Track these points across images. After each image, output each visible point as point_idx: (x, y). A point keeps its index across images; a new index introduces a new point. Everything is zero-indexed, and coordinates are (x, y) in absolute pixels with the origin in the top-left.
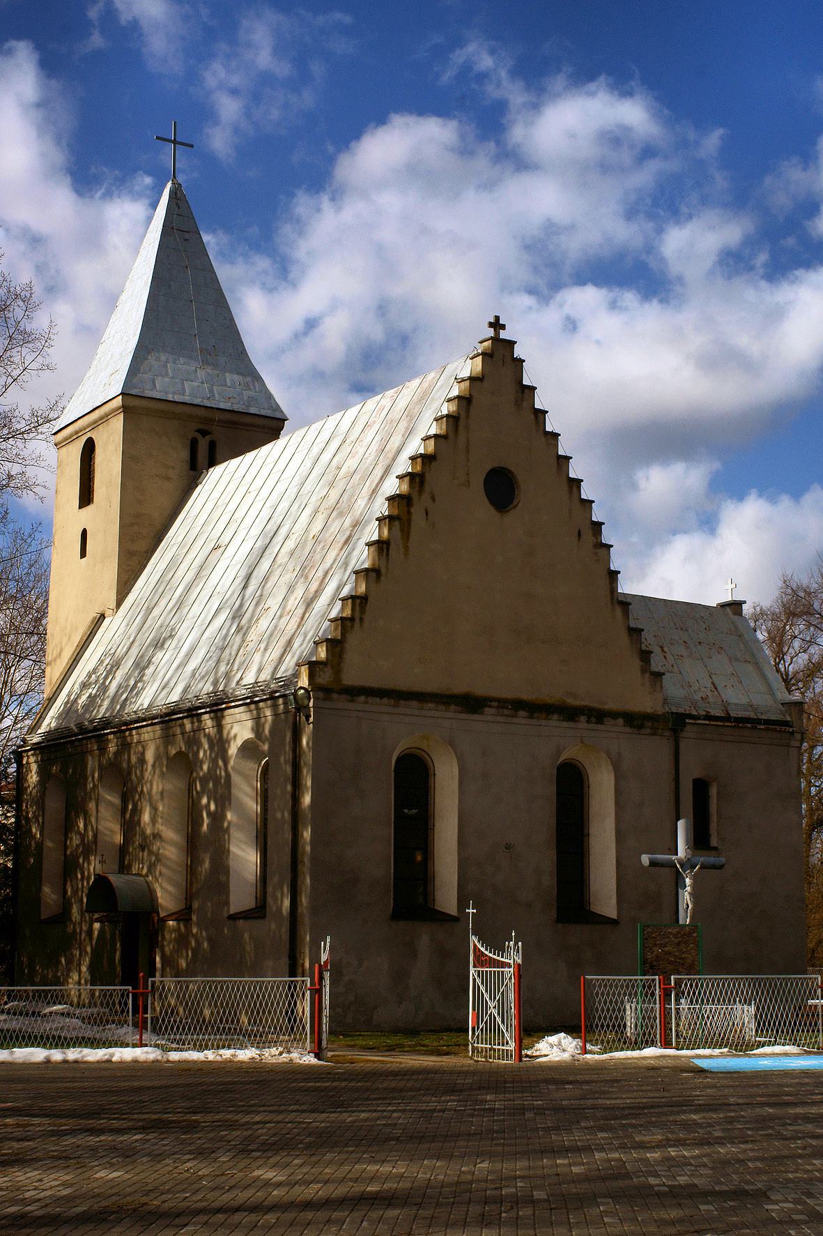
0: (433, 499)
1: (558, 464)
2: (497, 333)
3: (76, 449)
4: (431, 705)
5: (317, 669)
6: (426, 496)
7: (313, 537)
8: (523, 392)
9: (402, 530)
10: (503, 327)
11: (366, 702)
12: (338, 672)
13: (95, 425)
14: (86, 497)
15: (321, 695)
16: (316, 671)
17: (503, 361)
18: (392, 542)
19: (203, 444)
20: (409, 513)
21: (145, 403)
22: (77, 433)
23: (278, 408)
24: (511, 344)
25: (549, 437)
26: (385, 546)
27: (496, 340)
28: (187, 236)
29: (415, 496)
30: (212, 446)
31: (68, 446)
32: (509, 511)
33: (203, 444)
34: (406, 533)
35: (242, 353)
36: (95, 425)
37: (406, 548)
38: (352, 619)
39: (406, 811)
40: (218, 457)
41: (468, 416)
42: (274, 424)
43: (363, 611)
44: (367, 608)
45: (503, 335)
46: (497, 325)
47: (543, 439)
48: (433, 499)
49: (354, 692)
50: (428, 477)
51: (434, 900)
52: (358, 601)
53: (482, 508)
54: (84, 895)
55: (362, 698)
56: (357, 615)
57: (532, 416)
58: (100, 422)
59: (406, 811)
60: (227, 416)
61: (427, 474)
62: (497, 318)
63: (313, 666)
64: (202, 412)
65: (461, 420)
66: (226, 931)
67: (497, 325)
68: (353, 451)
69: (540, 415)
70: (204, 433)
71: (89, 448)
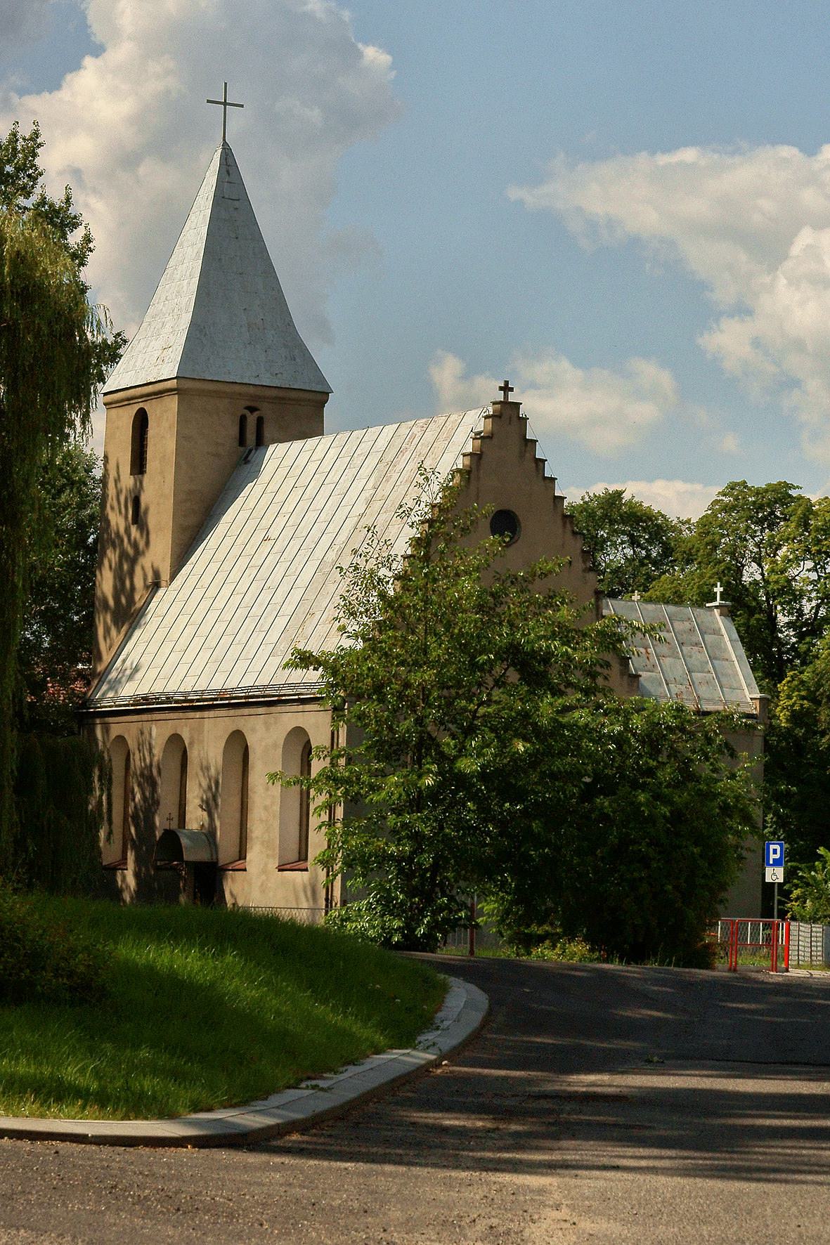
2: (506, 396)
3: (128, 415)
8: (526, 445)
14: (139, 464)
19: (252, 420)
21: (198, 385)
22: (128, 399)
23: (323, 380)
25: (548, 481)
27: (505, 403)
28: (237, 204)
30: (260, 421)
31: (120, 410)
33: (252, 420)
35: (289, 325)
40: (267, 434)
41: (478, 470)
42: (319, 397)
45: (512, 398)
54: (98, 793)
57: (534, 465)
60: (274, 393)
62: (507, 383)
64: (252, 390)
67: (506, 388)
68: (388, 475)
70: (252, 409)
71: (141, 422)
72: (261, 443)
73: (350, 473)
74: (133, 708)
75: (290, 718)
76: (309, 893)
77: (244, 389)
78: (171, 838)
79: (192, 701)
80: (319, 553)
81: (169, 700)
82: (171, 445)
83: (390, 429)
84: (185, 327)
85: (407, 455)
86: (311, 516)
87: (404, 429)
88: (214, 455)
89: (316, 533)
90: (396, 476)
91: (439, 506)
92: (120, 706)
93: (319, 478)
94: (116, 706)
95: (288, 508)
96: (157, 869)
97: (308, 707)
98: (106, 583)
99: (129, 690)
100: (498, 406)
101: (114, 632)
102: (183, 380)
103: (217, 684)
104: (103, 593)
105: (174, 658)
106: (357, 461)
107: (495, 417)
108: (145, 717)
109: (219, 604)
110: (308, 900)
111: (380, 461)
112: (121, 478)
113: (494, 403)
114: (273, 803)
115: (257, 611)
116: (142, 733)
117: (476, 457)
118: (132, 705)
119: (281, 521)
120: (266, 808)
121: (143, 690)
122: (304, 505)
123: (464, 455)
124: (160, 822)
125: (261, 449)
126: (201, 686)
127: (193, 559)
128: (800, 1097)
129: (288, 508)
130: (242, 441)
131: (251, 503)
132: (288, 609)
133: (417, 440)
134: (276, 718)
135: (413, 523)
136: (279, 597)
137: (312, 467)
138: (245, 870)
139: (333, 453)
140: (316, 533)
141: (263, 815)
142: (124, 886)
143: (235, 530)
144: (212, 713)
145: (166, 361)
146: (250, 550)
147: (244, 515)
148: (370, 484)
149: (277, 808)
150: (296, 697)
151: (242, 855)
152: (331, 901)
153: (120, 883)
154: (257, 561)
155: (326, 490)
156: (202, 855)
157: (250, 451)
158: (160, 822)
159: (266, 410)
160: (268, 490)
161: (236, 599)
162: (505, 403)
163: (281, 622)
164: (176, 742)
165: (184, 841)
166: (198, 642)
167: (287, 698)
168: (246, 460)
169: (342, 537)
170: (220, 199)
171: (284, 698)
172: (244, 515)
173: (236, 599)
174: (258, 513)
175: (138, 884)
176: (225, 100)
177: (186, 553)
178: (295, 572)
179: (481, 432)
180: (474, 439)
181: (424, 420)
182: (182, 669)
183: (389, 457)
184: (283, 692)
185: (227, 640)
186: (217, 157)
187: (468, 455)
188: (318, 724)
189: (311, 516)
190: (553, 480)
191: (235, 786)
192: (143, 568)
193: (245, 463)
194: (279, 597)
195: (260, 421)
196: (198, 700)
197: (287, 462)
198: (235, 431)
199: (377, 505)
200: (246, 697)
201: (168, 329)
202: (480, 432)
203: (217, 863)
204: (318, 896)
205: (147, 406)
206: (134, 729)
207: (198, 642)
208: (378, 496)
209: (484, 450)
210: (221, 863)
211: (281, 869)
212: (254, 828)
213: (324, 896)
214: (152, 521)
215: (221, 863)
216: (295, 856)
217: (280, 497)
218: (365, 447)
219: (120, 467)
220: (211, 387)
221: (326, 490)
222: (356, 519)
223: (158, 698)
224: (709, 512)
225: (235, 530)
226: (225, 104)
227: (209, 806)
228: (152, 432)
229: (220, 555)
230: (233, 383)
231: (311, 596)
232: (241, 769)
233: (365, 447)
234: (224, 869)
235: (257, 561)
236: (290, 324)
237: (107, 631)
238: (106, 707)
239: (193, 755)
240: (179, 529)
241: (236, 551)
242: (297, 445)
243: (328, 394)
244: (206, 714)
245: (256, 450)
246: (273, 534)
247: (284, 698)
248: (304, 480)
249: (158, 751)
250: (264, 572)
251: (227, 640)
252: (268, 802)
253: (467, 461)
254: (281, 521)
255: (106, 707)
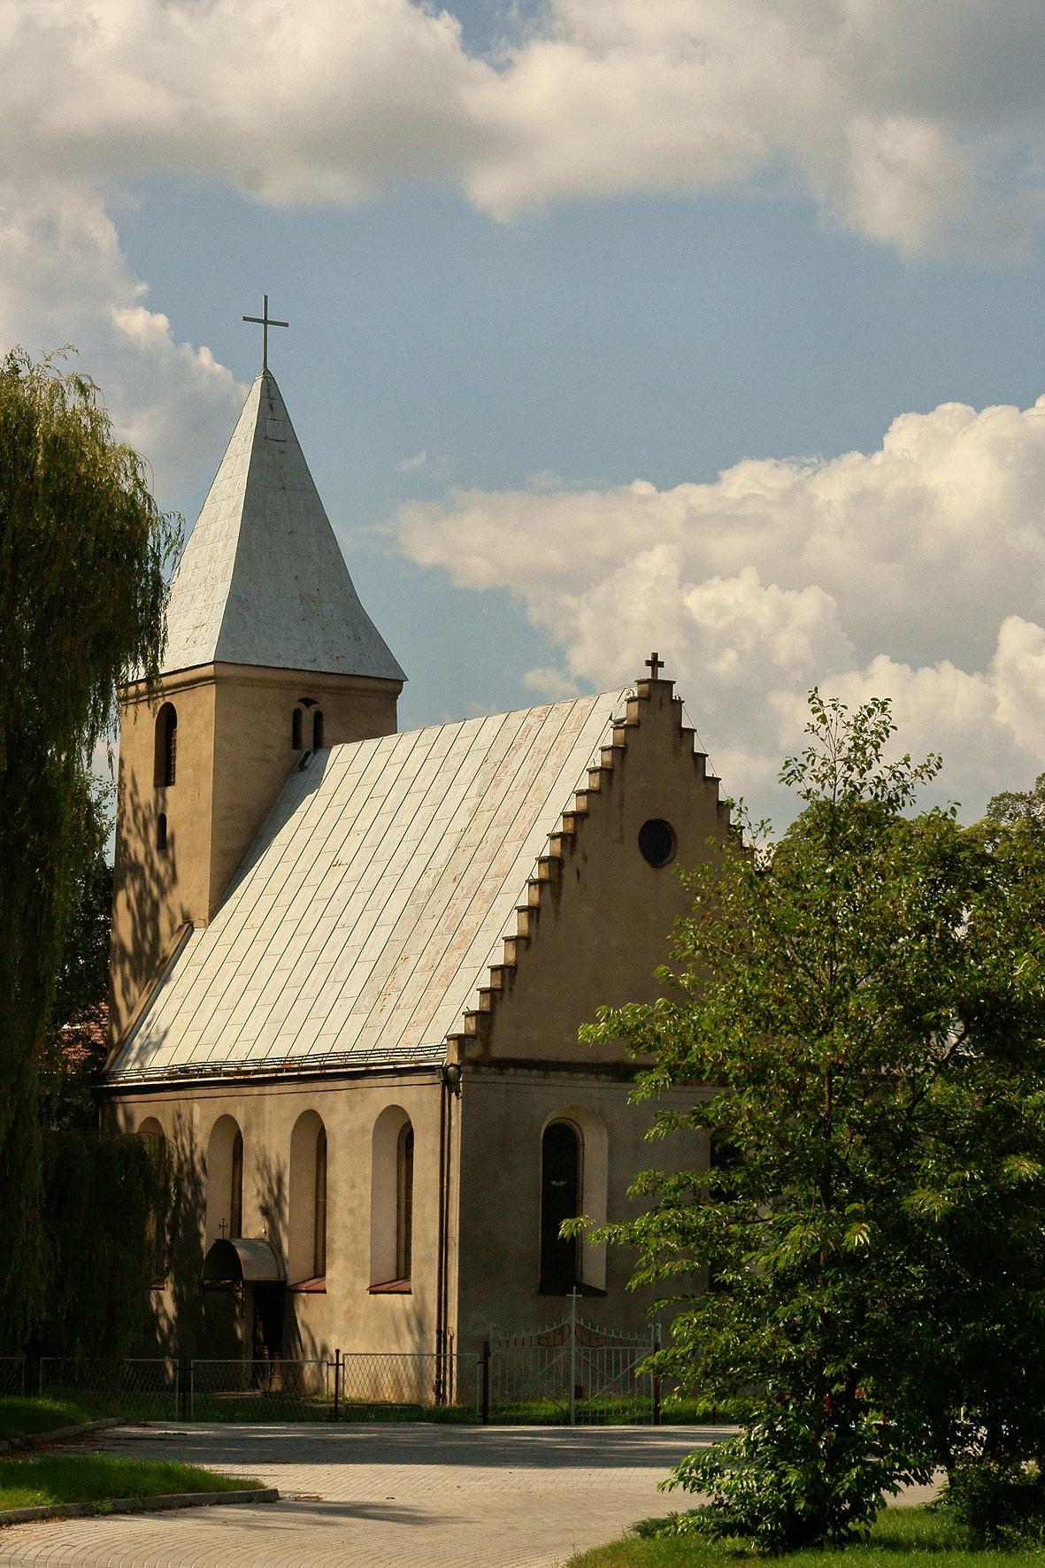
0: (585, 859)
1: (718, 812)
2: (654, 673)
4: (581, 1075)
5: (467, 1043)
6: (578, 857)
7: (455, 879)
8: (681, 736)
9: (552, 893)
10: (661, 665)
11: (515, 1075)
12: (487, 1045)
13: (176, 690)
14: (165, 773)
15: (470, 1068)
16: (465, 1044)
17: (661, 704)
18: (542, 908)
19: (308, 715)
20: (560, 876)
24: (670, 684)
26: (535, 913)
27: (654, 682)
29: (567, 856)
30: (318, 717)
32: (665, 865)
33: (308, 715)
34: (557, 898)
36: (176, 690)
37: (557, 912)
38: (502, 990)
39: (554, 1183)
40: (327, 734)
42: (390, 686)
43: (512, 981)
44: (518, 977)
45: (663, 674)
46: (655, 663)
47: (703, 785)
48: (585, 859)
49: (502, 1065)
50: (580, 837)
51: (582, 1273)
52: (507, 971)
53: (639, 866)
55: (512, 1071)
56: (507, 988)
57: (692, 761)
58: (183, 688)
59: (554, 1183)
61: (579, 834)
62: (655, 656)
63: (460, 1040)
64: (307, 678)
65: (616, 772)
66: (203, 1312)
69: (699, 759)
70: (308, 702)
72: (320, 744)
73: (444, 779)
74: (168, 1082)
75: (382, 1095)
76: (414, 1323)
77: (296, 677)
78: (224, 1251)
79: (248, 1072)
80: (409, 880)
81: (216, 1072)
82: (207, 747)
83: (495, 721)
84: (222, 599)
85: (522, 752)
86: (395, 834)
87: (515, 719)
88: (262, 760)
89: (403, 854)
90: (508, 779)
91: (574, 815)
92: (151, 1080)
93: (402, 786)
94: (146, 1080)
95: (363, 824)
96: (205, 1288)
97: (406, 1080)
98: (124, 928)
99: (160, 1060)
100: (645, 686)
101: (134, 989)
102: (221, 666)
103: (280, 1051)
104: (119, 937)
105: (220, 1017)
106: (454, 762)
107: (642, 700)
108: (182, 1094)
109: (277, 947)
110: (411, 1332)
111: (485, 761)
112: (139, 787)
113: (639, 682)
114: (361, 1206)
115: (329, 955)
116: (179, 1116)
117: (619, 751)
118: (167, 1079)
119: (354, 842)
120: (351, 1211)
121: (181, 1059)
122: (384, 820)
123: (603, 749)
124: (208, 1233)
125: (321, 753)
126: (258, 1053)
127: (239, 891)
128: (533, 1431)
129: (363, 824)
130: (296, 742)
131: (312, 820)
132: (372, 952)
133: (533, 734)
134: (362, 1095)
135: (808, 791)
136: (358, 938)
137: (392, 773)
138: (324, 1292)
139: (419, 754)
140: (403, 854)
141: (348, 1220)
142: (161, 1311)
143: (292, 855)
144: (275, 1089)
145: (199, 642)
146: (315, 878)
147: (303, 835)
148: (474, 789)
149: (366, 1211)
150: (392, 1067)
151: (319, 1271)
152: (445, 1333)
153: (154, 1307)
154: (325, 892)
155: (414, 800)
156: (267, 1273)
157: (307, 754)
158: (208, 1233)
159: (326, 703)
160: (335, 802)
161: (300, 942)
162: (654, 682)
163: (363, 970)
164: (226, 1123)
165: (241, 1252)
166: (251, 997)
167: (378, 1068)
168: (302, 766)
169: (440, 859)
170: (263, 440)
171: (374, 1068)
172: (303, 835)
173: (300, 942)
174: (322, 832)
175: (178, 1309)
176: (266, 317)
177: (229, 883)
178: (378, 905)
179: (623, 720)
180: (615, 729)
181: (542, 708)
182: (231, 1033)
183: (497, 755)
184: (371, 1061)
185: (289, 994)
186: (260, 380)
187: (609, 749)
188: (420, 1100)
189: (395, 834)
190: (716, 781)
191: (308, 1181)
192: (169, 909)
193: (301, 770)
194: (358, 938)
195: (318, 717)
196: (256, 1072)
197: (359, 765)
198: (287, 730)
199: (484, 818)
200: (321, 1068)
201: (199, 603)
202: (622, 721)
203: (286, 1281)
204: (426, 1328)
205: (174, 700)
206: (170, 1108)
207: (251, 997)
208: (485, 806)
209: (628, 742)
210: (290, 1283)
211: (374, 1291)
212: (335, 1238)
213: (435, 1327)
214: (181, 848)
215: (290, 1283)
216: (392, 1274)
217: (351, 811)
218: (462, 745)
219: (137, 779)
220: (258, 674)
221: (414, 800)
222: (458, 835)
223: (201, 1070)
224: (789, 837)
225: (292, 855)
226: (266, 322)
227: (270, 1212)
228: (182, 731)
229: (276, 885)
230: (283, 668)
231: (401, 934)
232: (313, 1164)
233: (462, 745)
234: (295, 1291)
235: (325, 892)
236: (352, 595)
237: (126, 990)
238: (132, 1081)
239: (250, 1141)
240: (219, 854)
241: (296, 880)
242: (370, 744)
243: (401, 682)
244: (267, 1089)
245: (315, 753)
246: (345, 857)
247: (374, 1068)
248: (382, 789)
249: (201, 1139)
250: (336, 906)
251: (289, 994)
252: (355, 1204)
253: (608, 757)
254: (354, 842)
255: (132, 1081)
